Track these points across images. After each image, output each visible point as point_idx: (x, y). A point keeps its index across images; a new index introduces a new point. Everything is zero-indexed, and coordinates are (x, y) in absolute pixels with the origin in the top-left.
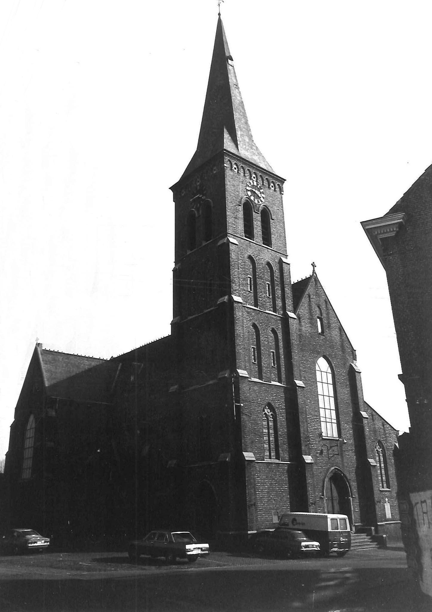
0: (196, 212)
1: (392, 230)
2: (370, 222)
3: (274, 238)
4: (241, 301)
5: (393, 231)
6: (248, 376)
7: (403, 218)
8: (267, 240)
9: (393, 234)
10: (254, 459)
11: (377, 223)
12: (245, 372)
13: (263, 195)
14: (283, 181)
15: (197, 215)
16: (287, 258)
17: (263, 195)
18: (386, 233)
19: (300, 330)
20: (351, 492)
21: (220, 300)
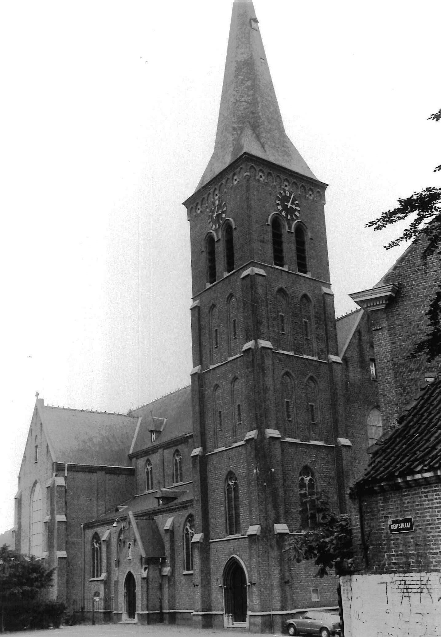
0: (215, 234)
1: (381, 303)
2: (362, 294)
3: (310, 263)
4: (271, 347)
5: (383, 304)
6: (280, 436)
7: (392, 291)
8: (303, 267)
9: (383, 307)
10: (288, 531)
11: (368, 295)
12: (277, 432)
13: (298, 209)
14: (323, 186)
15: (216, 239)
16: (330, 288)
17: (298, 209)
18: (378, 305)
19: (347, 376)
20: (192, 564)
21: (246, 345)
